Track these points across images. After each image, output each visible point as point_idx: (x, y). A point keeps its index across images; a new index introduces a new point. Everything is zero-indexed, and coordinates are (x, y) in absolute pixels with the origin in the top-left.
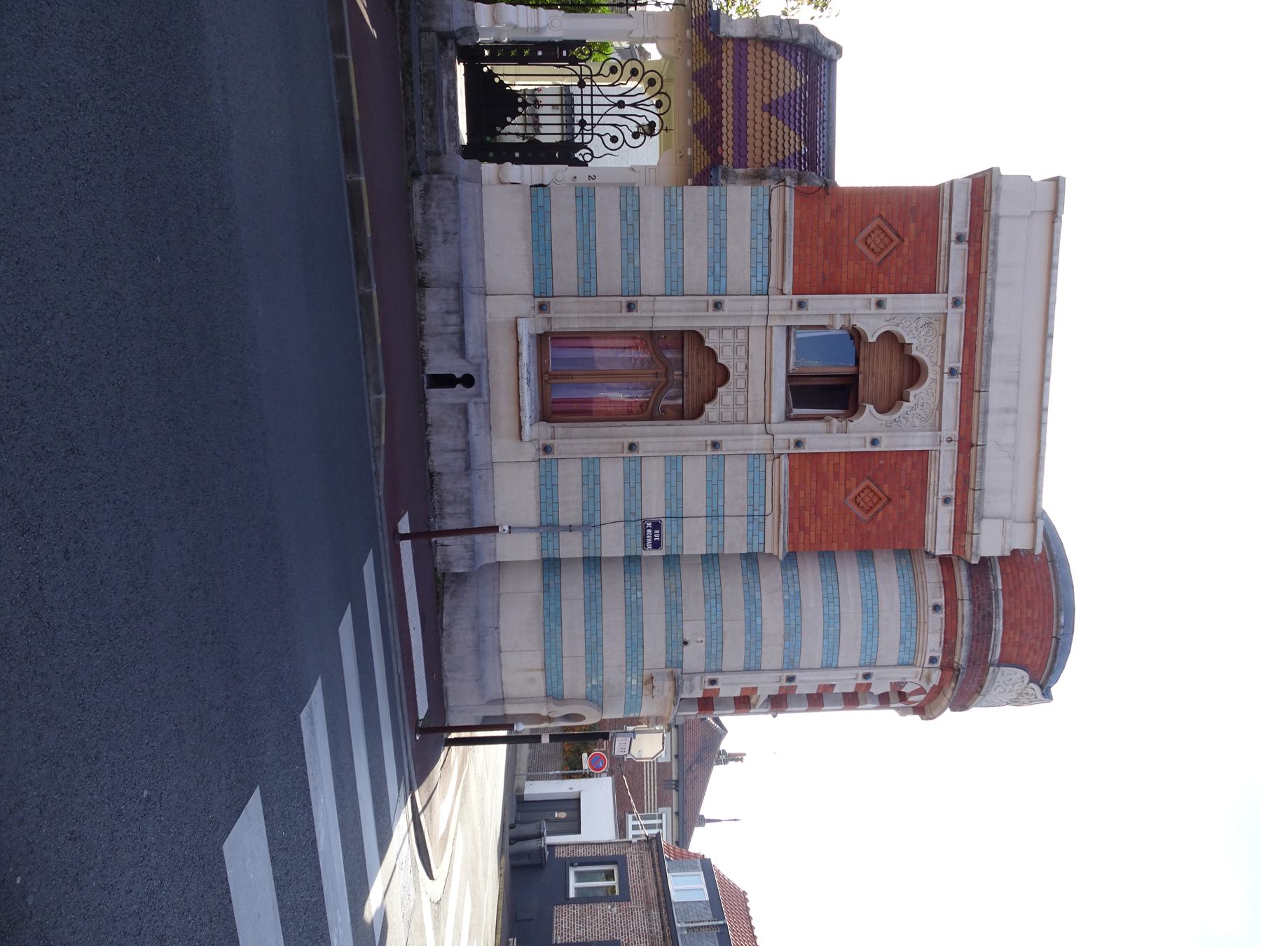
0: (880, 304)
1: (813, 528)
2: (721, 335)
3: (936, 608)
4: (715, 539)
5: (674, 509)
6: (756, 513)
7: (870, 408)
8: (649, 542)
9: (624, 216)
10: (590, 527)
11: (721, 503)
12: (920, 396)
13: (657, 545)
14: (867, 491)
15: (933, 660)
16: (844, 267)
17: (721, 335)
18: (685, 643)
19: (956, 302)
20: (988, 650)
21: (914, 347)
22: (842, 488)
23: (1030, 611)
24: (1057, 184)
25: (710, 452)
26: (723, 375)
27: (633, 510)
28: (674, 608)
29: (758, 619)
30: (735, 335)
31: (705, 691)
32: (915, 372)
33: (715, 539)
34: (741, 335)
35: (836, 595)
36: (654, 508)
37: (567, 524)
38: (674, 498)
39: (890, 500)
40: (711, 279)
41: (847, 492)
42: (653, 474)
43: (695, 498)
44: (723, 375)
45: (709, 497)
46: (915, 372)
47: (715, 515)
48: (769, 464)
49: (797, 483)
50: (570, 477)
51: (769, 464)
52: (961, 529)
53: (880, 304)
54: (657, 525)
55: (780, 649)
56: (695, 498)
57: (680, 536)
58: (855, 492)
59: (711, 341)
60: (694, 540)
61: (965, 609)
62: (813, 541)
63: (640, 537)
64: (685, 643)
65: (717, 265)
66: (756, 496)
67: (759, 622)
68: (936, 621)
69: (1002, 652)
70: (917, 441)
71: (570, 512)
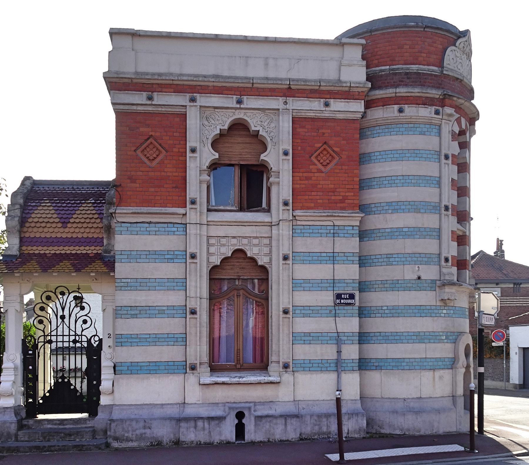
1: (342, 194)
2: (213, 254)
4: (349, 258)
5: (328, 285)
6: (332, 231)
7: (262, 157)
8: (350, 301)
9: (134, 316)
10: (338, 340)
13: (352, 296)
14: (319, 158)
16: (169, 174)
17: (213, 254)
18: (419, 278)
19: (193, 100)
22: (316, 175)
23: (406, 47)
24: (114, 33)
26: (239, 253)
29: (404, 230)
32: (239, 127)
33: (349, 258)
36: (327, 298)
39: (325, 143)
40: (175, 260)
44: (239, 253)
46: (239, 127)
47: (333, 258)
48: (299, 223)
53: (193, 151)
54: (339, 296)
55: (425, 215)
58: (320, 166)
59: (216, 260)
60: (349, 272)
61: (402, 91)
63: (346, 308)
64: (419, 278)
67: (406, 230)
68: (410, 110)
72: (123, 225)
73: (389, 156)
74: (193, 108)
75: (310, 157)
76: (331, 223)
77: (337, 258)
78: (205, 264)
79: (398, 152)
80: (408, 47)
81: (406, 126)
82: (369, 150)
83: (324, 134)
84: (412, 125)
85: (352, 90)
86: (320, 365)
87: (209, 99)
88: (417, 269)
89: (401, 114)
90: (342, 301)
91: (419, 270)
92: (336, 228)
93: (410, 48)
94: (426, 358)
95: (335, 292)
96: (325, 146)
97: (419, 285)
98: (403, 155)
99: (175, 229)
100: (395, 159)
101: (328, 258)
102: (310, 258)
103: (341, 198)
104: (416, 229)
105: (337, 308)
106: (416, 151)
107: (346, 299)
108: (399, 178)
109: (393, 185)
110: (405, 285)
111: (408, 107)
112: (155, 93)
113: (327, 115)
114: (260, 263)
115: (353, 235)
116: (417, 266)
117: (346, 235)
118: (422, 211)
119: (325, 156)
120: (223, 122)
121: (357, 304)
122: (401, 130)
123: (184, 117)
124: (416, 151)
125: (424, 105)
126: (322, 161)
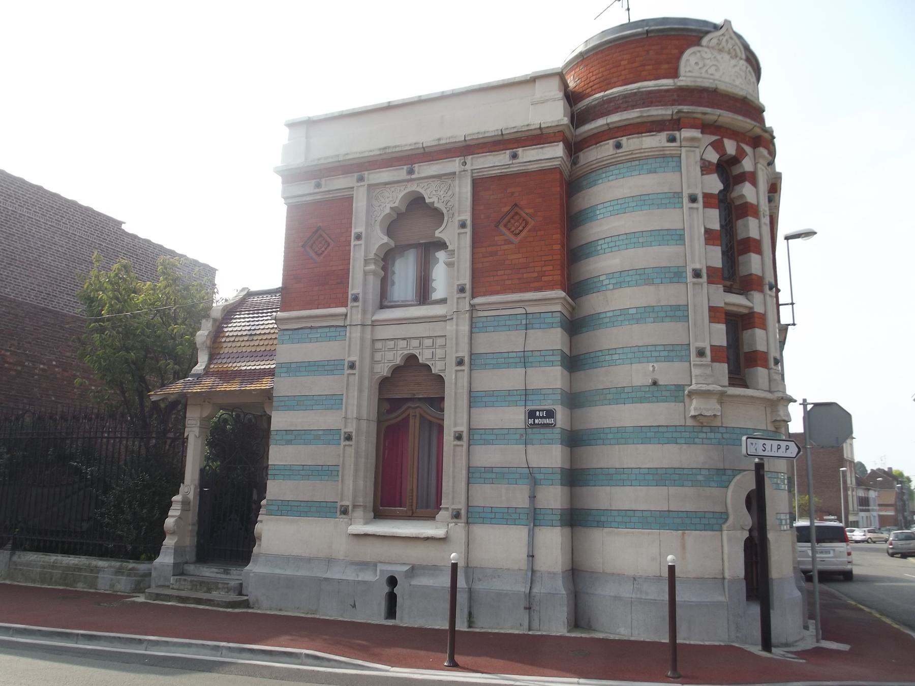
0: (359, 237)
1: (537, 269)
2: (378, 362)
3: (618, 146)
4: (547, 358)
5: (518, 398)
6: (524, 322)
7: (437, 234)
8: (547, 421)
9: (289, 442)
10: (533, 478)
11: (514, 355)
12: (433, 195)
13: (550, 414)
14: (509, 225)
15: (672, 139)
16: (334, 268)
17: (378, 362)
18: (655, 383)
19: (361, 179)
20: (660, 91)
21: (393, 205)
22: (504, 247)
23: (623, 63)
24: (292, 125)
25: (466, 368)
26: (411, 360)
27: (517, 436)
28: (622, 395)
29: (631, 311)
30: (379, 350)
31: (713, 360)
32: (417, 203)
33: (547, 358)
34: (379, 345)
35: (616, 238)
36: (515, 417)
37: (527, 500)
38: (507, 399)
39: (516, 205)
40: (335, 372)
41: (508, 242)
42: (488, 418)
43: (510, 379)
44: (411, 360)
45: (508, 365)
46: (417, 203)
47: (525, 360)
48: (481, 314)
49: (498, 288)
50: (489, 495)
51: (481, 314)
52: (539, 137)
53: (359, 237)
54: (532, 414)
55: (662, 287)
56: (510, 379)
57: (543, 392)
58: (510, 236)
59: (384, 370)
60: (552, 378)
61: (614, 118)
62: (551, 268)
63: (543, 431)
64: (655, 383)
65: (326, 368)
66: (508, 323)
67: (634, 311)
68: (630, 143)
69: (664, 77)
70: (466, 190)
71: (518, 497)
72: (286, 332)
73: (608, 209)
74: (361, 189)
75: (497, 226)
76: (522, 311)
77: (531, 359)
78: (366, 374)
79: (619, 202)
80: (626, 62)
81: (629, 164)
82: (593, 202)
83: (513, 193)
84: (637, 163)
85: (545, 131)
86: (506, 516)
87: (545, 150)
88: (651, 369)
89: (619, 151)
90: (537, 421)
91: (654, 370)
92: (530, 316)
93: (629, 63)
94: (669, 511)
95: (528, 408)
96: (517, 210)
97: (656, 394)
98: (626, 205)
99: (337, 334)
100: (616, 212)
101: (518, 360)
102: (494, 361)
103: (536, 275)
104: (648, 310)
105: (529, 431)
106: (643, 198)
107: (543, 417)
108: (621, 238)
109: (613, 249)
110: (633, 395)
111: (628, 139)
112: (416, 165)
113: (515, 169)
114: (435, 370)
115: (551, 326)
116: (651, 365)
117: (542, 326)
118: (656, 281)
119: (518, 221)
120: (393, 199)
121: (559, 424)
122: (622, 171)
123: (350, 199)
124: (643, 198)
125: (650, 132)
126: (513, 229)
